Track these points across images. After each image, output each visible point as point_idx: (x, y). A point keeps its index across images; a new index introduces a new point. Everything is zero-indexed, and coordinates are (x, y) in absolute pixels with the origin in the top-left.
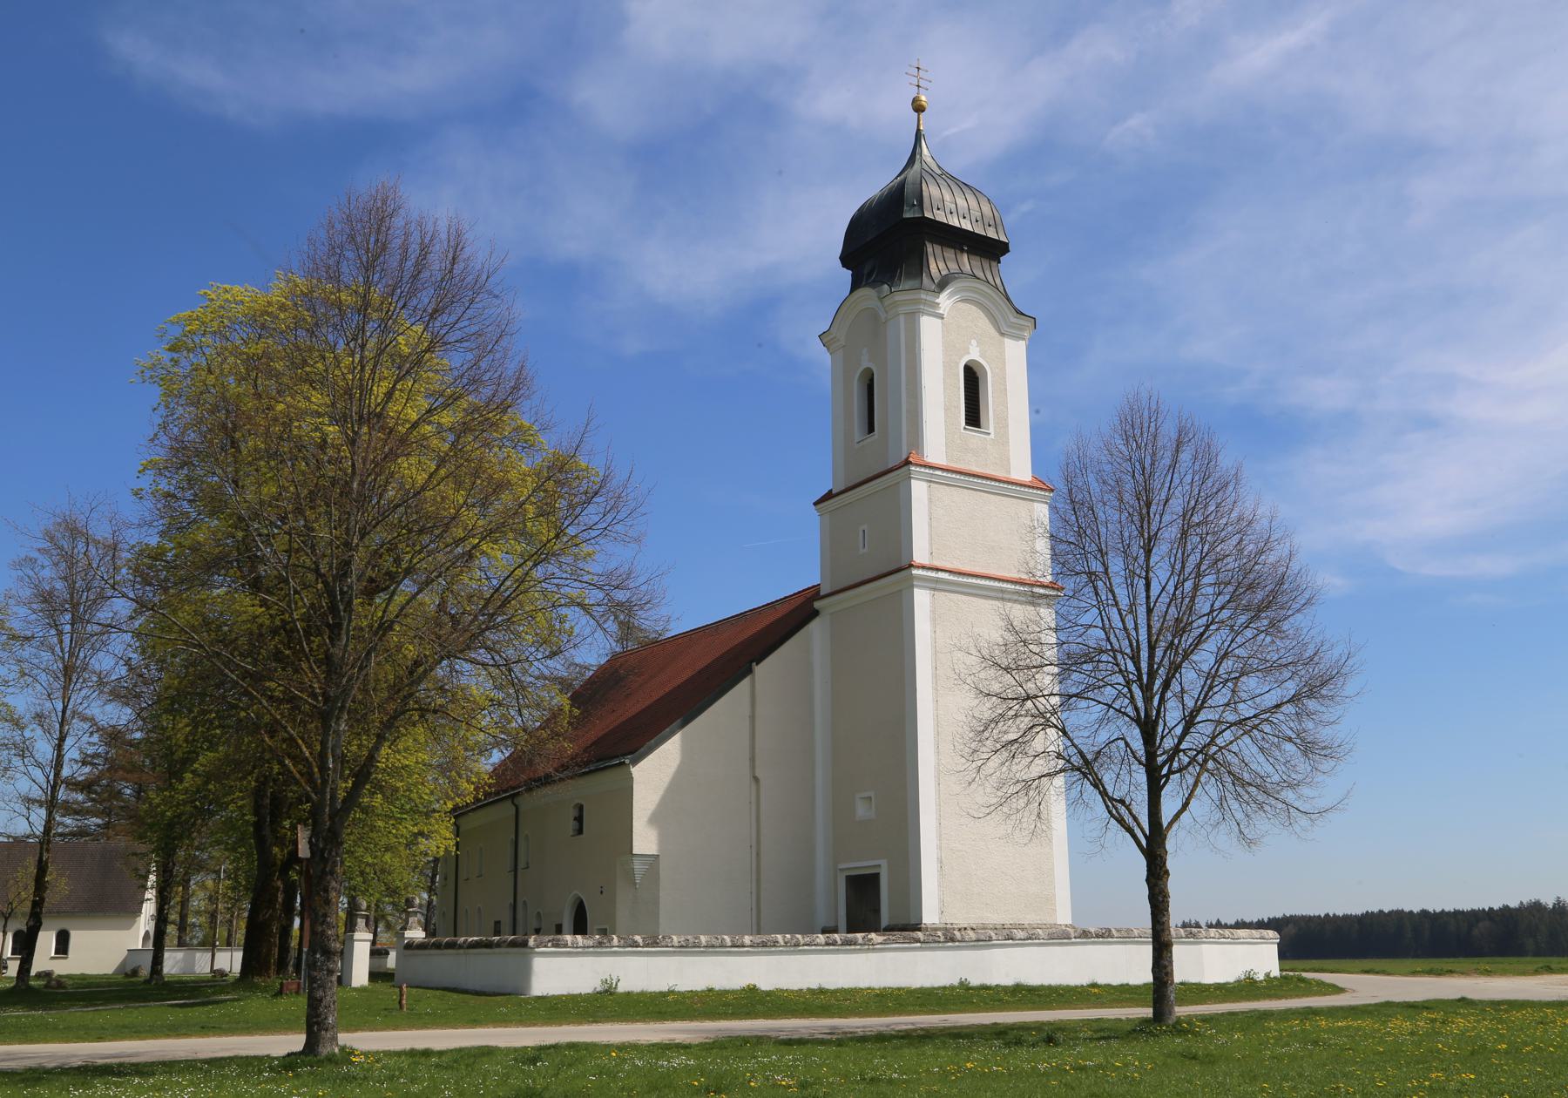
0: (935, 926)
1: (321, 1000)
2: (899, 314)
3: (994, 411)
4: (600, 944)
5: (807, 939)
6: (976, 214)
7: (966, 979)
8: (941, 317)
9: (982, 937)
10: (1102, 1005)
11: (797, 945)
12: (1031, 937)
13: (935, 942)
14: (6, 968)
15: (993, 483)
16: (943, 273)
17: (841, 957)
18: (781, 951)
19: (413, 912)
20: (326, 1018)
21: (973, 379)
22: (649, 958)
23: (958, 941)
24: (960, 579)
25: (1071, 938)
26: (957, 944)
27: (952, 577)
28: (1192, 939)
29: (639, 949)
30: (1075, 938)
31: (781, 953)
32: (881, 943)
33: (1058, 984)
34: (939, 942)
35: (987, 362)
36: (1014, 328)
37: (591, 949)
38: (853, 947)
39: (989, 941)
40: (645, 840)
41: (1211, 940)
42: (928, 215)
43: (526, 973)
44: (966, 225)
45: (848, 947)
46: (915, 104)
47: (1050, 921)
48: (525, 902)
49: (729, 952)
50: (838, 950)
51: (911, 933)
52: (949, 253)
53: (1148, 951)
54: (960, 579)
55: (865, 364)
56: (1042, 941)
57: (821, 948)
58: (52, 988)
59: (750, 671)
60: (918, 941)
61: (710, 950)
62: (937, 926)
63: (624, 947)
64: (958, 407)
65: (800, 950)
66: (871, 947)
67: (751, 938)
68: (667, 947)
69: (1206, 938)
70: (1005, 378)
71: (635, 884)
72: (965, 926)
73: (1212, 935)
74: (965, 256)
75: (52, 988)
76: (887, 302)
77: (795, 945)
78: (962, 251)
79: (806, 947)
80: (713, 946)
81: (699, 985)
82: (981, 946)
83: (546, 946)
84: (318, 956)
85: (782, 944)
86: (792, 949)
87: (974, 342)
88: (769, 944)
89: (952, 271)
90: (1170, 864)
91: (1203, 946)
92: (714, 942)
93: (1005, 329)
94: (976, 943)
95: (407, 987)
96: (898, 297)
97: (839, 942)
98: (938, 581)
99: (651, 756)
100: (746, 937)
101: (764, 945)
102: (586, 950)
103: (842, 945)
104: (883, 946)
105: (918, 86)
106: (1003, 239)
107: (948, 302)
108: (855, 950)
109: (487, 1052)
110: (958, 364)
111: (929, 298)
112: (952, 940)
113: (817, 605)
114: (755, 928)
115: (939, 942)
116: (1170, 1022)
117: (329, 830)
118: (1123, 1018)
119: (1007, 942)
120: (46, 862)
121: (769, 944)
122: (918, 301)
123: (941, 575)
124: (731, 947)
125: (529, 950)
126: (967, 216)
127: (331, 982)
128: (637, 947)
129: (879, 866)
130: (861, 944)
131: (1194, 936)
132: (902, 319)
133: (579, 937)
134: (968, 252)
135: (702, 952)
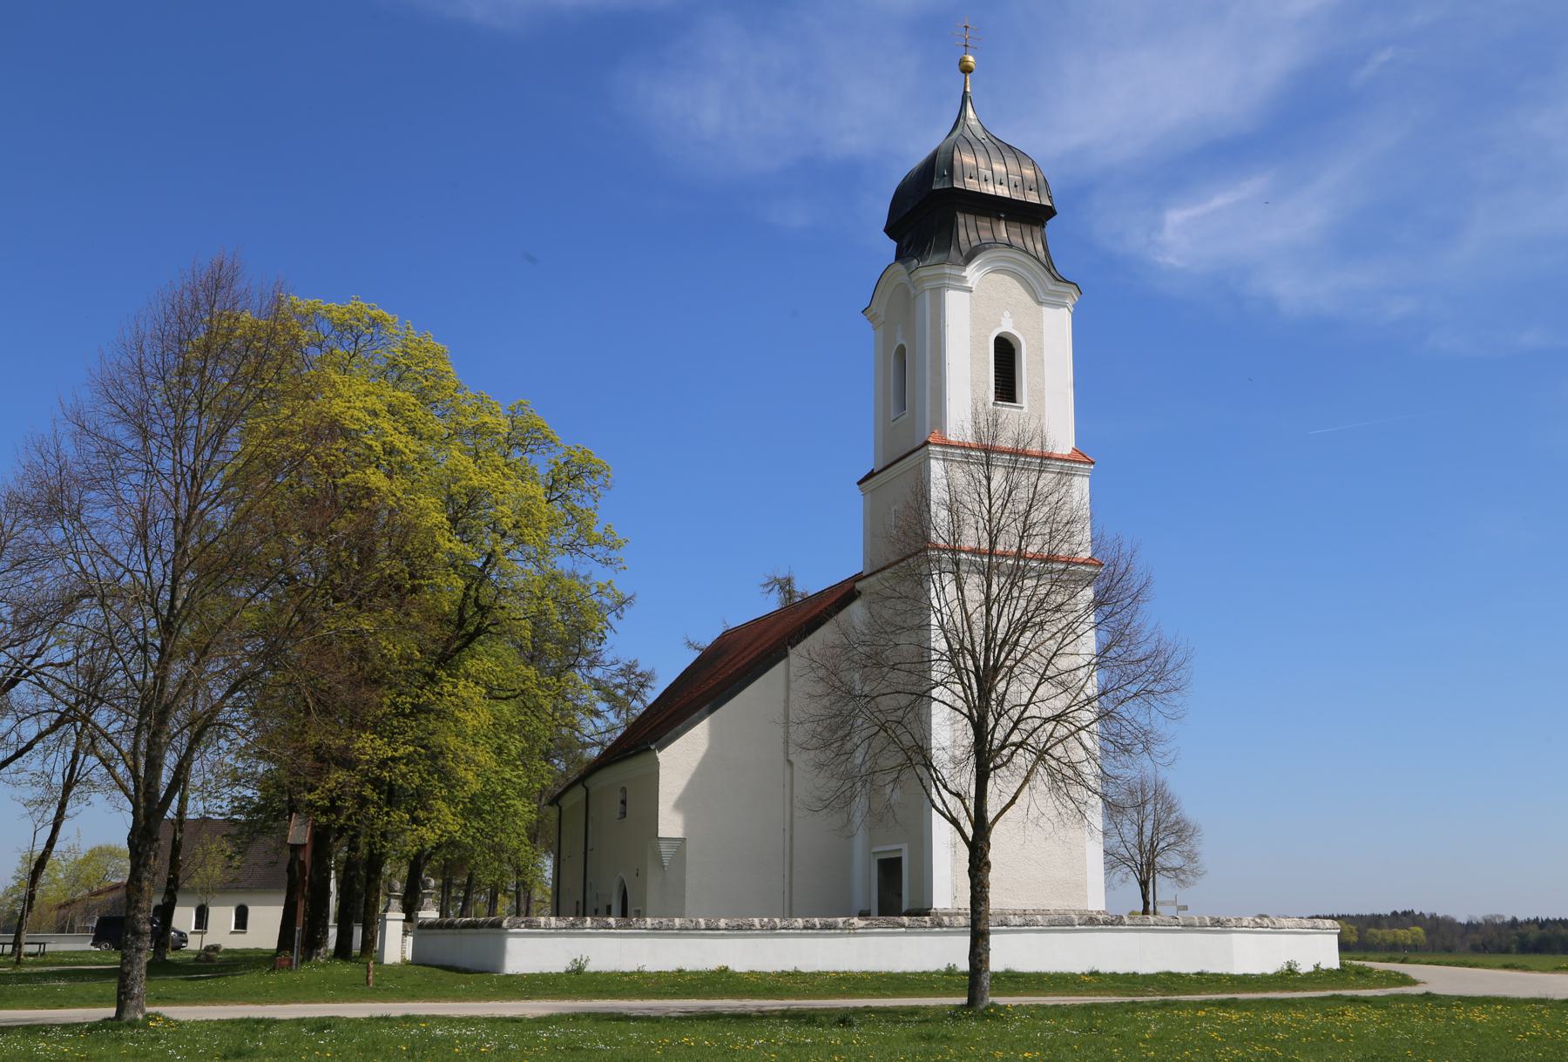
1: (128, 974)
2: (925, 290)
3: (1029, 383)
4: (573, 926)
5: (785, 923)
7: (954, 965)
8: (970, 290)
11: (774, 928)
12: (1062, 923)
13: (921, 927)
14: (186, 941)
16: (973, 244)
17: (821, 941)
18: (757, 934)
19: (428, 893)
20: (132, 989)
21: (1005, 352)
22: (623, 940)
23: (946, 927)
25: (1074, 925)
26: (945, 929)
28: (1219, 928)
29: (612, 931)
30: (1079, 925)
31: (757, 936)
32: (863, 928)
33: (1047, 971)
34: (925, 927)
35: (1021, 333)
36: (1054, 296)
37: (564, 931)
38: (833, 931)
40: (670, 825)
41: (1244, 929)
43: (500, 952)
44: (1003, 191)
45: (827, 931)
47: (1079, 906)
48: (591, 883)
50: (817, 934)
51: (896, 918)
52: (984, 223)
53: (965, 942)
55: (900, 341)
56: (1041, 927)
57: (799, 931)
58: (201, 961)
59: (785, 655)
60: (903, 926)
61: (684, 932)
63: (596, 928)
66: (852, 931)
67: (727, 921)
68: (640, 929)
69: (1236, 926)
70: (1042, 349)
71: (664, 866)
73: (1328, 926)
74: (1002, 225)
75: (201, 961)
76: (915, 277)
78: (999, 219)
79: (783, 931)
80: (687, 929)
81: (629, 965)
83: (519, 927)
84: (129, 936)
85: (759, 927)
86: (769, 932)
87: (1007, 314)
89: (983, 242)
90: (991, 856)
91: (1233, 935)
92: (688, 924)
93: (1043, 297)
95: (374, 963)
96: (923, 273)
97: (818, 926)
99: (677, 742)
100: (722, 920)
101: (739, 928)
102: (559, 931)
103: (821, 929)
106: (1046, 202)
108: (834, 934)
109: (271, 1023)
112: (940, 925)
113: (859, 586)
115: (925, 927)
116: (981, 1007)
117: (144, 828)
118: (1024, 1004)
120: (180, 841)
122: (943, 276)
125: (503, 931)
126: (1005, 182)
127: (139, 958)
128: (610, 928)
129: (901, 849)
130: (841, 929)
132: (927, 294)
133: (553, 919)
134: (1006, 219)
135: (677, 934)
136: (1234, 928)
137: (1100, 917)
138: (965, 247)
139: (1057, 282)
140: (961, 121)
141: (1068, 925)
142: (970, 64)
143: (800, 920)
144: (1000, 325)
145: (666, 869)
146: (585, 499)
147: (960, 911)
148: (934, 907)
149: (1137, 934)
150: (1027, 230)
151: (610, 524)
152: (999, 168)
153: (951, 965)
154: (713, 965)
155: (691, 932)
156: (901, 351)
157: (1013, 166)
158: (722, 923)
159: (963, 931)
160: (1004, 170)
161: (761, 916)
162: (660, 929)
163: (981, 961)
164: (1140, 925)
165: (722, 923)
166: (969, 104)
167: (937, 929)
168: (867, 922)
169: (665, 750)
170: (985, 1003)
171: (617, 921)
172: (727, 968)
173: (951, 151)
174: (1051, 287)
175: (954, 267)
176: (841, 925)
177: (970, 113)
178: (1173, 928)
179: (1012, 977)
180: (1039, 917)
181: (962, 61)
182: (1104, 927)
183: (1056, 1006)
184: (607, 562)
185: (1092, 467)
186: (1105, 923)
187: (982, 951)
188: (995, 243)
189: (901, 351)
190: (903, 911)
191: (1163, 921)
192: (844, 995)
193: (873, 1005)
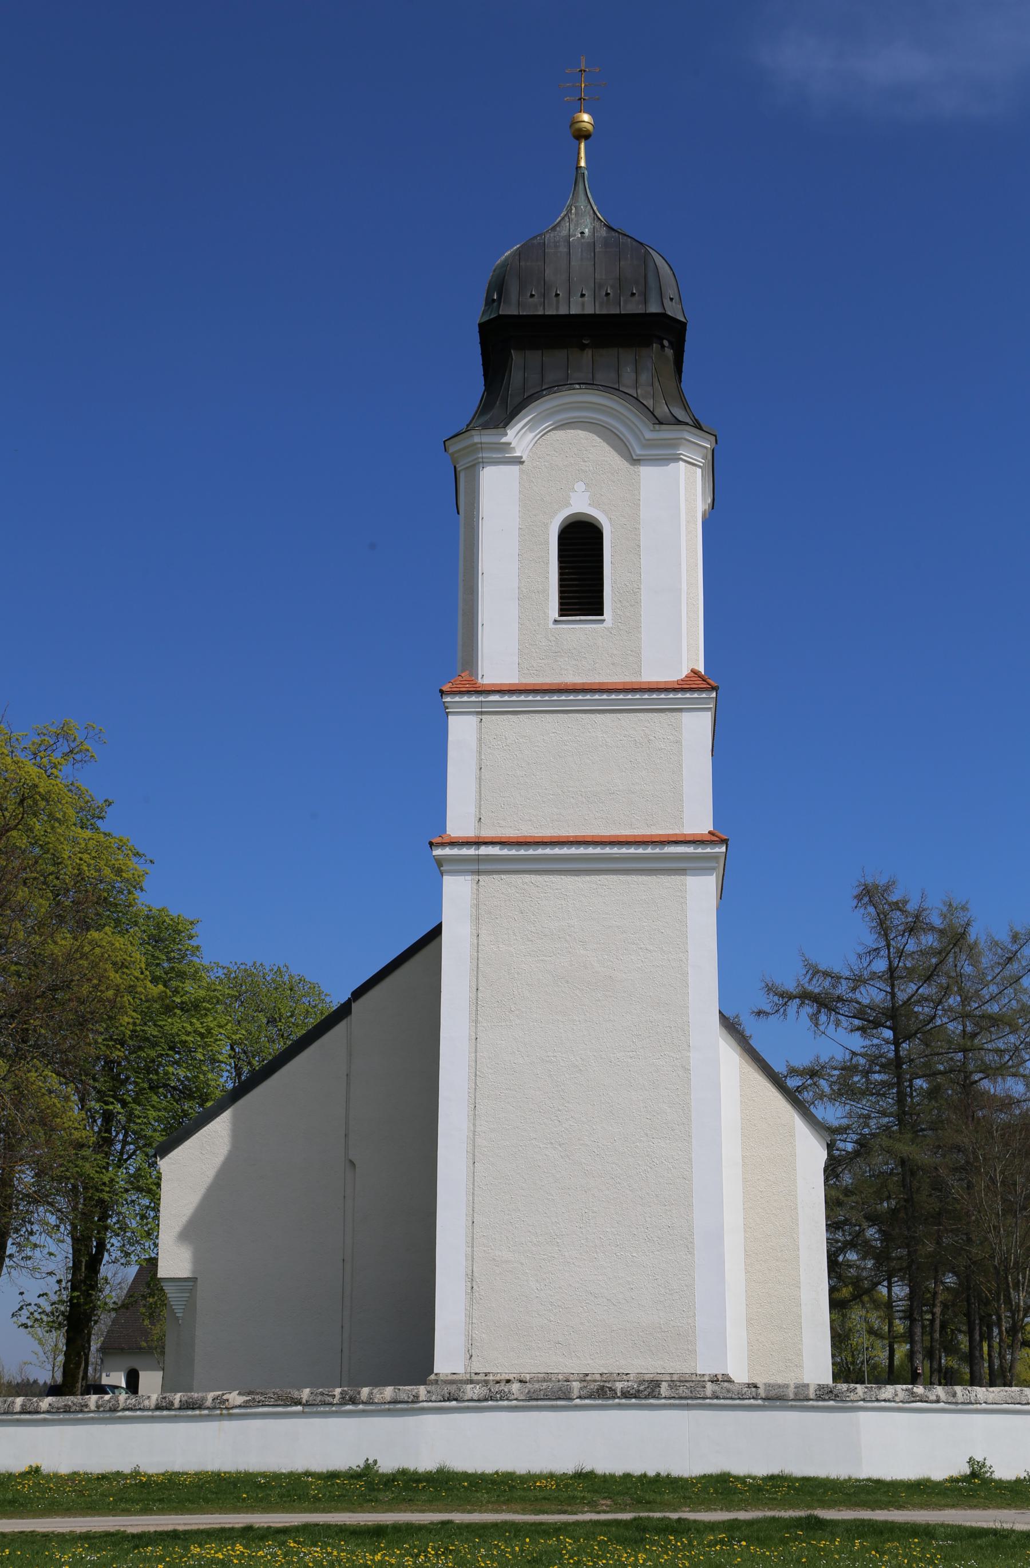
7: (375, 1462)
8: (519, 461)
9: (403, 1396)
11: (114, 1410)
23: (363, 1403)
24: (700, 850)
25: (571, 1399)
26: (361, 1407)
27: (506, 852)
28: (831, 1403)
30: (580, 1397)
32: (240, 1406)
38: (197, 1412)
39: (413, 1402)
41: (883, 1404)
45: (190, 1413)
49: (18, 1420)
50: (175, 1416)
54: (700, 850)
56: (514, 1403)
57: (150, 1413)
60: (298, 1403)
65: (120, 1418)
66: (224, 1412)
69: (864, 1400)
71: (177, 1319)
72: (511, 1377)
78: (583, 347)
79: (127, 1413)
82: (402, 1410)
87: (580, 486)
91: (862, 1415)
94: (391, 1406)
98: (479, 859)
101: (67, 1410)
103: (180, 1409)
104: (243, 1411)
107: (531, 435)
108: (201, 1416)
110: (546, 526)
119: (447, 1404)
122: (475, 448)
123: (484, 850)
124: (21, 1413)
130: (208, 1408)
136: (861, 1403)
137: (619, 1386)
139: (657, 427)
141: (559, 1399)
145: (180, 1321)
147: (475, 1377)
148: (435, 1371)
149: (684, 1414)
153: (370, 1461)
158: (305, 1394)
159: (389, 1410)
164: (686, 1398)
167: (349, 1407)
168: (248, 1398)
169: (170, 1155)
174: (649, 435)
175: (664, 427)
178: (746, 1402)
182: (623, 1401)
183: (591, 1521)
185: (714, 695)
186: (626, 1395)
191: (728, 1391)
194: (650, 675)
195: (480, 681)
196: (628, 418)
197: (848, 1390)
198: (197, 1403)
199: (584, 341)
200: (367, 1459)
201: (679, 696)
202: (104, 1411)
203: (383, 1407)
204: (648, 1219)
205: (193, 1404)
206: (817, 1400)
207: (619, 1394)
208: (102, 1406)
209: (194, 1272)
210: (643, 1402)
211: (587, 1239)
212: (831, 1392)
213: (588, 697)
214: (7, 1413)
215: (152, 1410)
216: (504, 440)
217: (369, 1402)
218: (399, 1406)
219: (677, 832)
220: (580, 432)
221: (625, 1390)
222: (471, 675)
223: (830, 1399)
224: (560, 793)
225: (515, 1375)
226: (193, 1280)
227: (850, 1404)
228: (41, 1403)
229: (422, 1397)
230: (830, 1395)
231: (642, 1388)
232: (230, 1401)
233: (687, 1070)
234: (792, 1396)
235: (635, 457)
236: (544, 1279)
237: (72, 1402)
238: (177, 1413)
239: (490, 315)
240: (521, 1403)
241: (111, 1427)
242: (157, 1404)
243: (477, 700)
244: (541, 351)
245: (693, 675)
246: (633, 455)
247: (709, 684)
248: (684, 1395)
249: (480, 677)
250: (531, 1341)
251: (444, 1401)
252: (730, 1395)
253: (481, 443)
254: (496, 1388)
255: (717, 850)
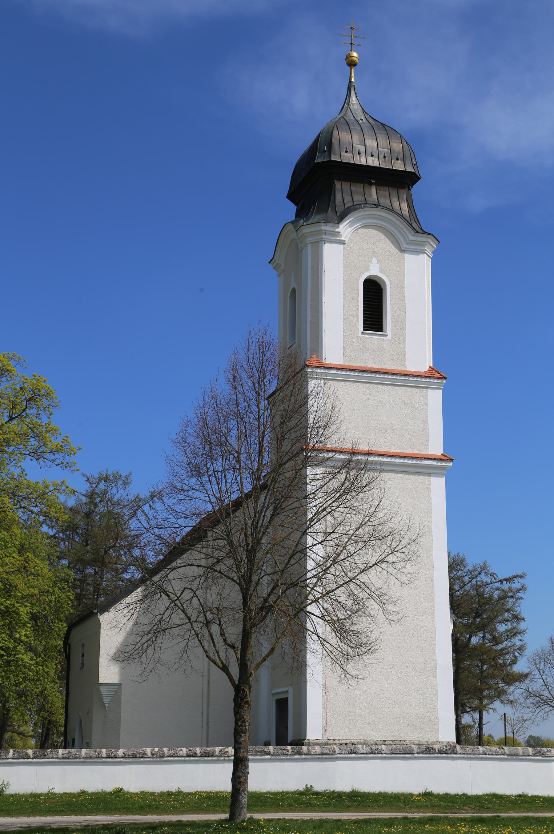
0: (318, 741)
6: (384, 150)
7: (311, 786)
8: (343, 243)
9: (327, 751)
10: (167, 813)
11: (162, 756)
13: (283, 754)
15: (386, 376)
16: (347, 206)
22: (38, 767)
23: (305, 754)
24: (439, 464)
25: (413, 754)
26: (303, 756)
28: (540, 758)
30: (418, 753)
31: (149, 763)
34: (287, 755)
38: (211, 758)
39: (332, 754)
42: (334, 158)
44: (373, 162)
45: (206, 758)
46: (347, 61)
49: (104, 762)
50: (198, 760)
52: (358, 188)
53: (229, 767)
54: (439, 464)
55: (293, 285)
56: (384, 755)
57: (183, 759)
60: (268, 754)
62: (320, 741)
63: (17, 758)
64: (357, 316)
65: (165, 761)
66: (226, 758)
68: (53, 758)
70: (404, 288)
72: (347, 742)
74: (373, 190)
77: (160, 757)
78: (371, 184)
79: (170, 758)
80: (91, 758)
81: (41, 788)
85: (150, 755)
87: (374, 261)
88: (138, 755)
89: (355, 203)
93: (405, 246)
94: (320, 756)
96: (305, 230)
97: (199, 754)
101: (134, 756)
103: (201, 756)
105: (351, 44)
106: (410, 169)
107: (350, 229)
108: (212, 760)
109: (327, 821)
110: (357, 280)
111: (329, 228)
114: (204, 742)
119: (350, 755)
121: (138, 755)
122: (321, 232)
124: (106, 758)
128: (28, 758)
130: (217, 756)
131: (541, 754)
132: (309, 247)
134: (377, 185)
135: (83, 762)
137: (436, 747)
138: (340, 209)
139: (416, 234)
140: (346, 106)
141: (407, 753)
142: (354, 59)
143: (184, 750)
144: (368, 270)
145: (106, 708)
146: (40, 416)
147: (329, 742)
148: (307, 738)
149: (469, 762)
150: (394, 192)
151: (67, 435)
152: (371, 143)
153: (309, 786)
154: (109, 787)
155: (94, 760)
156: (294, 291)
157: (383, 140)
159: (319, 758)
160: (375, 144)
161: (152, 746)
162: (69, 758)
163: (240, 783)
164: (470, 754)
165: (120, 752)
166: (353, 92)
170: (242, 817)
171: (34, 752)
172: (122, 789)
173: (331, 131)
174: (411, 238)
175: (420, 234)
176: (217, 753)
177: (353, 98)
179: (353, 796)
180: (384, 747)
181: (348, 56)
182: (439, 755)
184: (67, 466)
185: (444, 381)
186: (440, 752)
187: (241, 775)
188: (365, 204)
189: (294, 291)
190: (289, 742)
191: (491, 751)
192: (207, 811)
193: (38, 817)
194: (410, 368)
195: (323, 361)
196: (401, 228)
197: (547, 751)
198: (210, 753)
199: (372, 181)
200: (307, 785)
201: (428, 380)
202: (156, 757)
203: (316, 757)
204: (414, 659)
205: (208, 754)
206: (533, 756)
207: (437, 752)
208: (155, 754)
209: (120, 680)
210: (449, 756)
211: (384, 668)
212: (540, 752)
213: (382, 376)
214: (98, 758)
215: (185, 757)
216: (337, 230)
217: (308, 754)
218: (325, 756)
219: (426, 453)
220: (374, 231)
221: (440, 749)
222: (317, 357)
223: (539, 756)
224: (367, 427)
225: (349, 741)
226: (119, 685)
227: (549, 758)
228: (118, 752)
229: (337, 752)
230: (539, 754)
231: (448, 748)
232: (229, 752)
233: (432, 580)
234: (521, 754)
235: (403, 249)
236: (362, 689)
237: (136, 752)
238: (199, 759)
239: (324, 159)
240: (388, 755)
241: (159, 766)
242: (187, 754)
243: (325, 372)
244: (349, 183)
245: (431, 369)
246: (402, 247)
247: (441, 375)
248: (469, 752)
249: (323, 359)
250: (356, 723)
251: (349, 754)
252: (491, 753)
253: (326, 230)
254: (374, 747)
255: (448, 464)
